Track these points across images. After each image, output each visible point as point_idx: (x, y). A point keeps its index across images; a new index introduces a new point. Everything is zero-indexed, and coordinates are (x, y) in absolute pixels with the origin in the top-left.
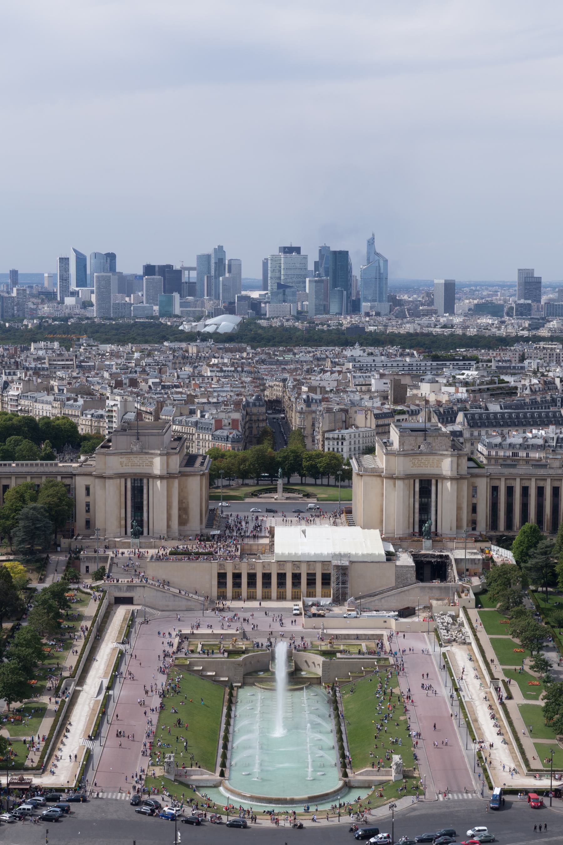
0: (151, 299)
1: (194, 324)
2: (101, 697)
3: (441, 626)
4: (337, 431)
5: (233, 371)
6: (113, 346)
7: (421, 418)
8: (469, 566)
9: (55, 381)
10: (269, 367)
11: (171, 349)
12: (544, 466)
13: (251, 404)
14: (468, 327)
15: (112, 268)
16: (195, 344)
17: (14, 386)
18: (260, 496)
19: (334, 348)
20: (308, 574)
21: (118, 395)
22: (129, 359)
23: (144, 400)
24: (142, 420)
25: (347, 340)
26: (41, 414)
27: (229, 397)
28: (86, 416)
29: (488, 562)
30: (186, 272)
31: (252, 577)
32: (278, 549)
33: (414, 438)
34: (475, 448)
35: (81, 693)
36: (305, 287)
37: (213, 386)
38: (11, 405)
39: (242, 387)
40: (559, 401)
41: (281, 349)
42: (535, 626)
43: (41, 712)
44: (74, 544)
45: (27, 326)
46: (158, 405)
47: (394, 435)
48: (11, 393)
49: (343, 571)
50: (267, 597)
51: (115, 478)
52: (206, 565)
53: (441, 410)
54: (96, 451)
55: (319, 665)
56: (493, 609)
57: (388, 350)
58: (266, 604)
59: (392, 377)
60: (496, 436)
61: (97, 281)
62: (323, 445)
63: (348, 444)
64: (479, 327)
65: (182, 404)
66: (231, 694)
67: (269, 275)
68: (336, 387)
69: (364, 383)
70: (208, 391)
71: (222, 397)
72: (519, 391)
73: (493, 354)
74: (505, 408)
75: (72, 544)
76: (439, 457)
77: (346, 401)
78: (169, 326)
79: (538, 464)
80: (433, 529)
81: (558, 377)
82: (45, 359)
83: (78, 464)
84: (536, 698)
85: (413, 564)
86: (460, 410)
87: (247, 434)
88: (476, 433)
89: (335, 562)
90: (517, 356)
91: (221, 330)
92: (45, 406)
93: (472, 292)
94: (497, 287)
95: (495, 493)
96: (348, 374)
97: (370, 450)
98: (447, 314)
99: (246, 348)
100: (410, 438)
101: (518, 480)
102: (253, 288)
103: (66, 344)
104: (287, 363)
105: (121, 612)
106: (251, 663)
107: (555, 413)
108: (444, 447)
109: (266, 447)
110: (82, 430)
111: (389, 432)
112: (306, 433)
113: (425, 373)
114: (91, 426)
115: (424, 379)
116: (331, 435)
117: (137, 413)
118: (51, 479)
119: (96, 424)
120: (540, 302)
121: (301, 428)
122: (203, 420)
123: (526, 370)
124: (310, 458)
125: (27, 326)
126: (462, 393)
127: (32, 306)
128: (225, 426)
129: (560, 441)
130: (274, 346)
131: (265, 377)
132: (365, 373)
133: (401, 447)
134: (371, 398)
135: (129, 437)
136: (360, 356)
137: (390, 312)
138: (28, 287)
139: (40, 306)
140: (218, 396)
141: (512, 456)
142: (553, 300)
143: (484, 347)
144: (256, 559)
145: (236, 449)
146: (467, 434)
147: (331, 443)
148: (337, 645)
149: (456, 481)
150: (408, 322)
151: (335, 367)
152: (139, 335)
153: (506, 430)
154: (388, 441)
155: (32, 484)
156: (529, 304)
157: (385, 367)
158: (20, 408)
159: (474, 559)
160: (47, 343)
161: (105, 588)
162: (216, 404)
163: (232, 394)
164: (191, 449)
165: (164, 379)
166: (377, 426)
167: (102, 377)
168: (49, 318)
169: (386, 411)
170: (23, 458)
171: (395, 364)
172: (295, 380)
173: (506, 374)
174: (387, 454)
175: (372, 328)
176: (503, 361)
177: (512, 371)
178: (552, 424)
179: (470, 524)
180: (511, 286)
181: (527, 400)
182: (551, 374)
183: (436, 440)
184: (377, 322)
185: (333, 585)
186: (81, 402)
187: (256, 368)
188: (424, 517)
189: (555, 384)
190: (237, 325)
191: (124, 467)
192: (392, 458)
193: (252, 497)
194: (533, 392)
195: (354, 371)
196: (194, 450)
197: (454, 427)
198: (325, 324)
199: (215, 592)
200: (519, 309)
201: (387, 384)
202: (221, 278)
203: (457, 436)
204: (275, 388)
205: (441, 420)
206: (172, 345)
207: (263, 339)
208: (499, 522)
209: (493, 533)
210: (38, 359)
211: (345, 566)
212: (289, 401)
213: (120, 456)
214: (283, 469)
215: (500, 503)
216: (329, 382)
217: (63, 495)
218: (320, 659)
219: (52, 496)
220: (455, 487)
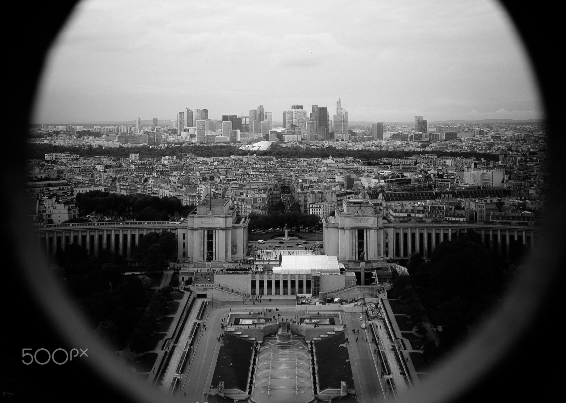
1: (247, 146)
12: (423, 222)
14: (389, 146)
15: (206, 117)
16: (247, 157)
20: (299, 281)
21: (203, 185)
26: (163, 195)
30: (244, 119)
31: (269, 283)
35: (176, 348)
38: (148, 190)
39: (268, 180)
41: (291, 159)
44: (177, 266)
46: (224, 190)
49: (317, 279)
51: (199, 230)
52: (245, 276)
54: (189, 216)
56: (397, 300)
59: (346, 175)
79: (421, 221)
81: (432, 174)
82: (168, 165)
84: (418, 349)
85: (355, 275)
86: (381, 192)
87: (270, 205)
88: (389, 204)
91: (261, 149)
92: (166, 190)
93: (392, 128)
101: (409, 229)
102: (275, 127)
103: (180, 158)
106: (268, 330)
113: (364, 172)
114: (189, 201)
126: (382, 183)
129: (432, 208)
130: (288, 157)
138: (163, 127)
142: (434, 132)
143: (395, 158)
146: (384, 204)
153: (404, 202)
156: (421, 134)
158: (152, 191)
164: (241, 213)
166: (338, 201)
175: (339, 148)
177: (410, 170)
178: (429, 199)
179: (385, 253)
180: (412, 125)
181: (416, 186)
182: (429, 172)
185: (313, 287)
186: (184, 188)
189: (430, 177)
195: (327, 171)
199: (250, 291)
210: (164, 165)
211: (318, 277)
220: (376, 233)
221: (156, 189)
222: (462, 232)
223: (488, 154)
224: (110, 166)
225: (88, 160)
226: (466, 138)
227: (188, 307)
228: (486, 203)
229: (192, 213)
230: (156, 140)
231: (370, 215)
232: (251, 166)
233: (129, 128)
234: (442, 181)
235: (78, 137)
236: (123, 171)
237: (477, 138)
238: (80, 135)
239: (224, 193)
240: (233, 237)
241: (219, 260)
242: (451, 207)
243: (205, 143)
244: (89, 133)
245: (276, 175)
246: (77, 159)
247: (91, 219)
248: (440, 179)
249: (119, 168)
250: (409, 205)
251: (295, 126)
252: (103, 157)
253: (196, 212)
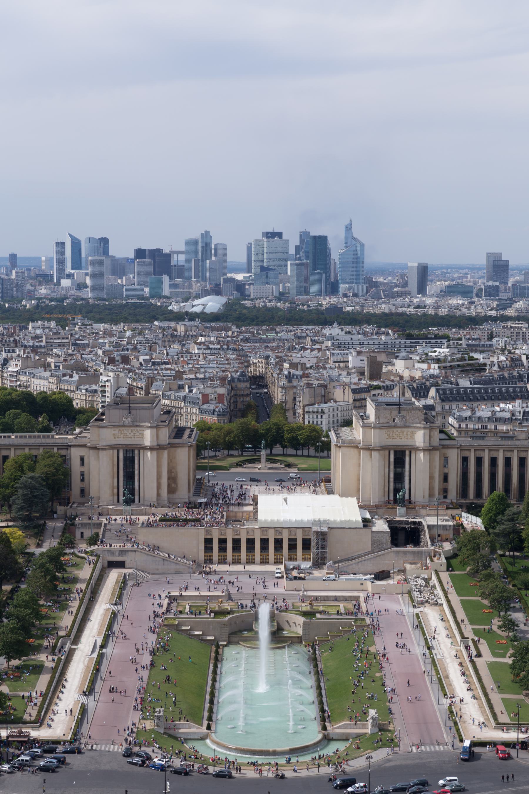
0: (142, 281)
1: (182, 304)
2: (95, 655)
3: (414, 588)
4: (317, 405)
5: (219, 349)
6: (106, 325)
7: (396, 393)
8: (441, 532)
9: (52, 358)
10: (253, 344)
11: (160, 328)
12: (512, 438)
13: (236, 380)
14: (440, 307)
15: (106, 252)
16: (183, 323)
17: (13, 362)
18: (245, 466)
19: (314, 327)
20: (290, 540)
21: (111, 371)
22: (121, 337)
23: (135, 375)
24: (133, 395)
25: (326, 319)
26: (38, 389)
27: (215, 373)
28: (81, 391)
29: (459, 528)
30: (175, 256)
31: (237, 543)
32: (261, 516)
33: (389, 411)
34: (446, 421)
35: (77, 652)
36: (287, 269)
37: (200, 363)
38: (11, 381)
39: (228, 364)
40: (525, 376)
41: (264, 328)
43: (38, 669)
44: (70, 511)
45: (25, 306)
46: (148, 380)
47: (371, 409)
48: (10, 369)
49: (322, 536)
50: (251, 561)
51: (109, 449)
52: (193, 531)
53: (415, 385)
54: (91, 424)
55: (300, 625)
56: (463, 573)
57: (365, 329)
58: (250, 568)
59: (368, 355)
60: (466, 409)
61: (91, 264)
62: (304, 418)
63: (327, 417)
64: (450, 307)
65: (171, 380)
66: (217, 653)
67: (253, 259)
68: (316, 364)
69: (342, 360)
70: (195, 368)
71: (209, 373)
72: (487, 367)
73: (463, 332)
74: (475, 383)
75: (68, 511)
76: (413, 430)
77: (325, 377)
78: (159, 306)
79: (506, 436)
80: (407, 497)
81: (524, 354)
82: (42, 337)
83: (74, 436)
84: (504, 656)
85: (389, 530)
86: (432, 385)
87: (232, 408)
88: (447, 407)
89: (315, 528)
90: (486, 334)
91: (208, 310)
92: (42, 381)
93: (444, 274)
94: (467, 270)
95: (465, 463)
96: (327, 351)
97: (348, 423)
98: (420, 296)
99: (231, 327)
100: (386, 411)
101: (487, 451)
102: (238, 270)
104: (269, 341)
105: (114, 575)
106: (235, 623)
107: (521, 388)
108: (417, 420)
110: (77, 404)
111: (366, 406)
112: (287, 407)
113: (399, 350)
114: (86, 400)
115: (398, 356)
116: (311, 409)
117: (129, 388)
118: (48, 450)
119: (90, 398)
120: (508, 284)
121: (283, 402)
122: (191, 395)
123: (494, 347)
124: (292, 430)
125: (25, 306)
126: (435, 369)
127: (30, 288)
128: (211, 400)
129: (526, 414)
130: (257, 325)
131: (249, 355)
132: (343, 350)
133: (377, 420)
134: (349, 374)
135: (121, 410)
136: (338, 334)
137: (367, 293)
138: (27, 269)
139: (38, 288)
140: (205, 372)
141: (481, 428)
142: (520, 282)
144: (241, 525)
145: (222, 422)
146: (438, 408)
147: (311, 416)
148: (316, 606)
149: (428, 452)
150: (383, 303)
151: (315, 345)
152: (130, 314)
153: (475, 404)
154: (365, 414)
155: (30, 455)
156: (497, 286)
157: (361, 344)
158: (18, 383)
159: (446, 526)
160: (44, 322)
161: (99, 553)
162: (203, 380)
163: (218, 370)
164: (179, 422)
165: (154, 356)
166: (355, 400)
167: (96, 354)
168: (46, 299)
169: (362, 386)
170: (22, 430)
171: (371, 342)
172: (277, 357)
173: (476, 351)
174: (363, 427)
175: (349, 309)
176: (473, 339)
177: (481, 349)
178: (519, 399)
179: (442, 493)
180: (480, 269)
181: (496, 376)
183: (410, 414)
184: (354, 303)
185: (313, 549)
186: (76, 377)
187: (241, 346)
188: (399, 486)
189: (521, 361)
190: (223, 306)
191: (117, 439)
192: (368, 430)
193: (237, 467)
194: (501, 368)
195: (333, 349)
196: (182, 422)
197: (426, 401)
198: (305, 305)
199: (202, 556)
200: (488, 290)
201: (363, 360)
202: (208, 262)
203: (430, 410)
204: (258, 364)
205: (414, 395)
206: (162, 324)
207: (247, 318)
208: (469, 490)
209: (463, 501)
210: (36, 337)
211: (324, 532)
212: (271, 377)
213: (113, 429)
214: (266, 441)
215: (470, 473)
216: (309, 359)
217: (60, 465)
218: (301, 620)
219: (49, 466)
220: (428, 457)
221: (25, 378)
253: (104, 417)
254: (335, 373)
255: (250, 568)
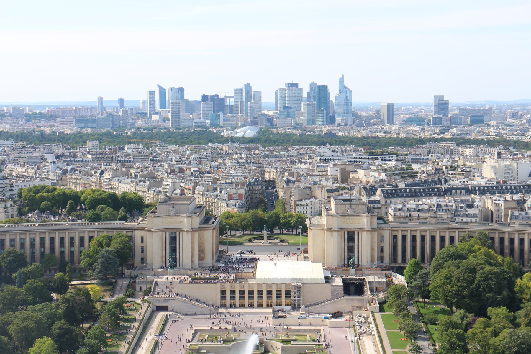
0: (206, 117)
1: (230, 132)
3: (357, 324)
4: (303, 201)
7: (355, 192)
8: (378, 286)
13: (252, 184)
14: (400, 132)
16: (227, 145)
22: (183, 155)
23: (187, 181)
24: (184, 194)
25: (323, 141)
26: (123, 190)
27: (239, 179)
30: (228, 99)
31: (242, 293)
32: (258, 276)
36: (301, 108)
37: (231, 172)
39: (248, 173)
41: (280, 148)
42: (412, 324)
44: (134, 273)
45: (127, 133)
48: (105, 177)
49: (298, 289)
53: (368, 187)
55: (279, 348)
64: (408, 133)
67: (279, 100)
69: (324, 170)
72: (419, 174)
74: (408, 186)
75: (132, 273)
80: (356, 263)
82: (131, 155)
85: (342, 285)
86: (380, 187)
87: (249, 202)
89: (293, 284)
91: (247, 136)
92: (126, 185)
95: (395, 240)
97: (320, 214)
98: (389, 124)
99: (258, 147)
105: (160, 316)
107: (438, 189)
109: (260, 212)
110: (148, 200)
111: (330, 202)
116: (299, 203)
118: (119, 233)
119: (157, 197)
120: (448, 116)
121: (283, 198)
122: (221, 194)
124: (285, 217)
125: (127, 133)
126: (383, 176)
127: (131, 121)
128: (234, 197)
129: (439, 207)
130: (278, 145)
134: (326, 180)
137: (354, 123)
139: (137, 121)
142: (456, 114)
144: (245, 282)
145: (241, 212)
146: (383, 202)
147: (299, 208)
148: (291, 336)
150: (363, 130)
152: (195, 139)
153: (407, 199)
155: (107, 236)
158: (110, 187)
159: (381, 281)
161: (150, 301)
163: (241, 177)
164: (213, 212)
165: (201, 168)
167: (163, 167)
169: (334, 188)
171: (346, 157)
174: (327, 216)
175: (341, 134)
177: (421, 161)
179: (379, 259)
181: (423, 181)
185: (292, 298)
186: (147, 183)
192: (330, 218)
195: (320, 163)
199: (219, 302)
200: (435, 120)
202: (249, 103)
204: (271, 172)
209: (394, 265)
210: (127, 155)
217: (126, 243)
218: (280, 345)
220: (369, 236)
222: (471, 234)
223: (520, 141)
224: (63, 156)
225: (36, 148)
226: (495, 122)
227: (145, 320)
228: (506, 201)
229: (152, 212)
230: (121, 125)
231: (341, 215)
232: (230, 156)
233: (89, 110)
234: (455, 174)
235: (27, 121)
236: (77, 161)
237: (509, 122)
238: (30, 117)
239: (194, 188)
240: (201, 239)
241: (184, 267)
242: (462, 205)
243: (180, 129)
244: (41, 116)
245: (259, 167)
246: (23, 147)
247: (33, 219)
248: (453, 172)
249: (73, 158)
250: (411, 204)
251: (289, 108)
252: (55, 144)
253: (156, 211)
254: (317, 179)
255: (232, 311)
